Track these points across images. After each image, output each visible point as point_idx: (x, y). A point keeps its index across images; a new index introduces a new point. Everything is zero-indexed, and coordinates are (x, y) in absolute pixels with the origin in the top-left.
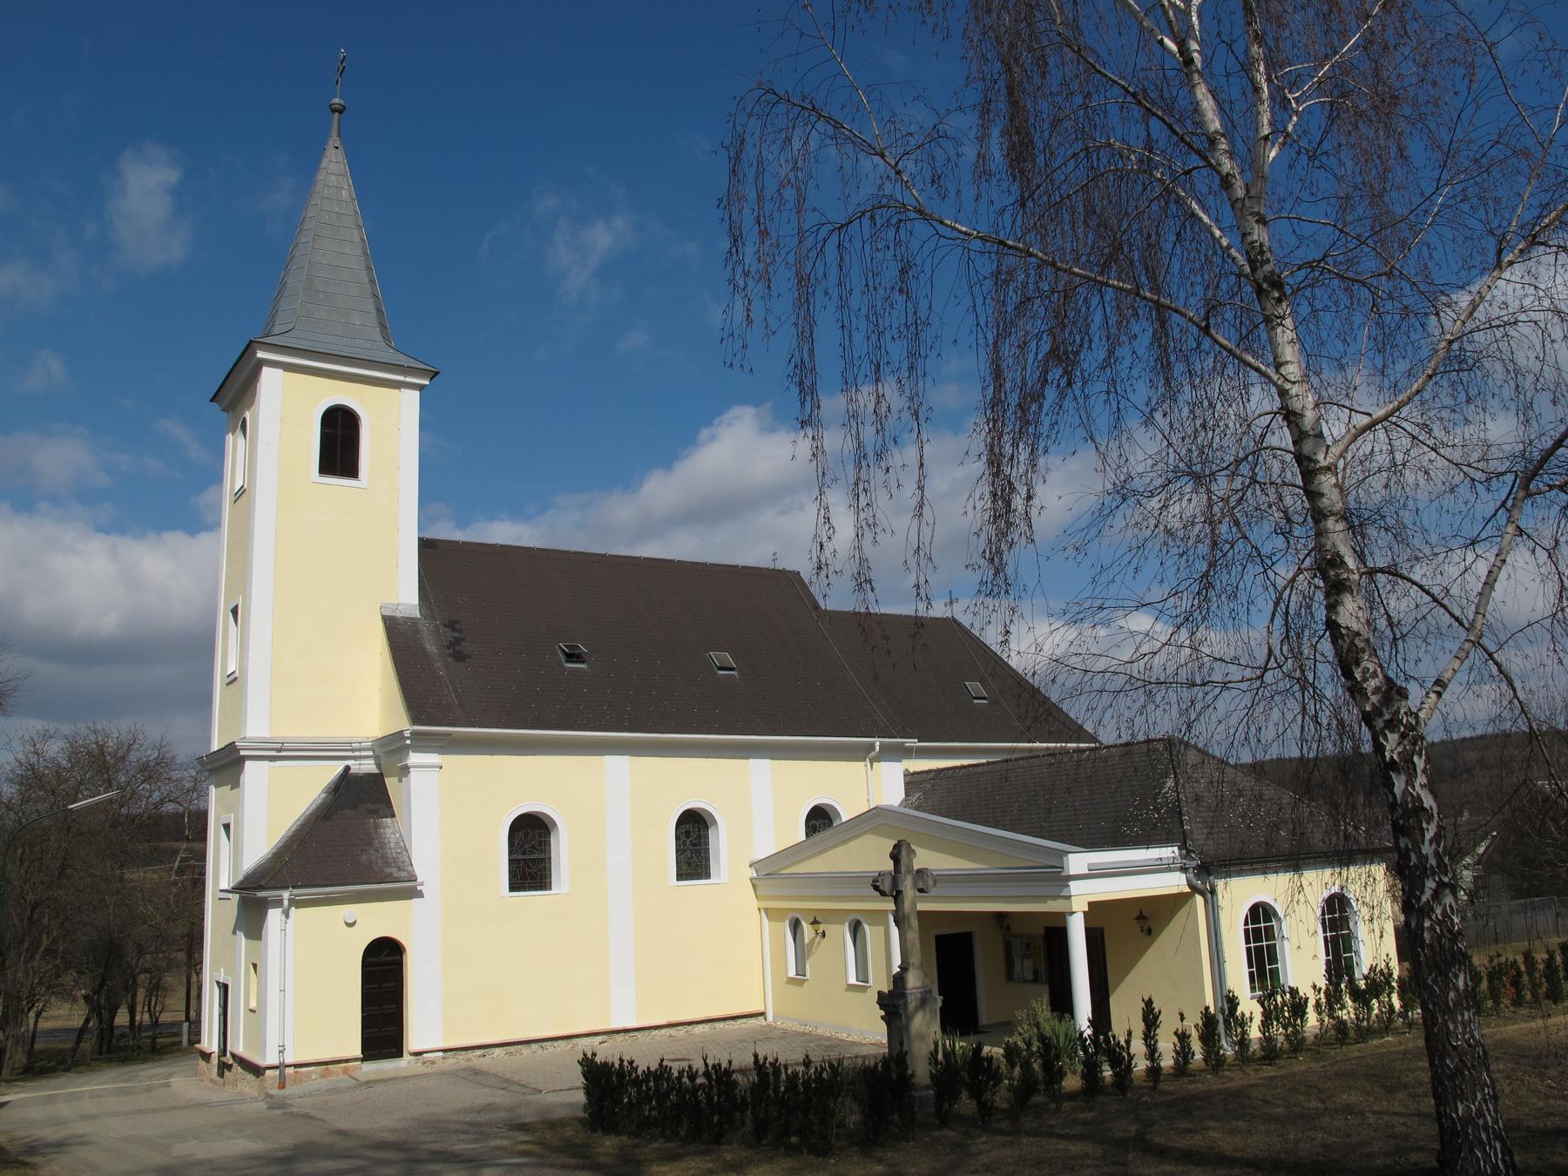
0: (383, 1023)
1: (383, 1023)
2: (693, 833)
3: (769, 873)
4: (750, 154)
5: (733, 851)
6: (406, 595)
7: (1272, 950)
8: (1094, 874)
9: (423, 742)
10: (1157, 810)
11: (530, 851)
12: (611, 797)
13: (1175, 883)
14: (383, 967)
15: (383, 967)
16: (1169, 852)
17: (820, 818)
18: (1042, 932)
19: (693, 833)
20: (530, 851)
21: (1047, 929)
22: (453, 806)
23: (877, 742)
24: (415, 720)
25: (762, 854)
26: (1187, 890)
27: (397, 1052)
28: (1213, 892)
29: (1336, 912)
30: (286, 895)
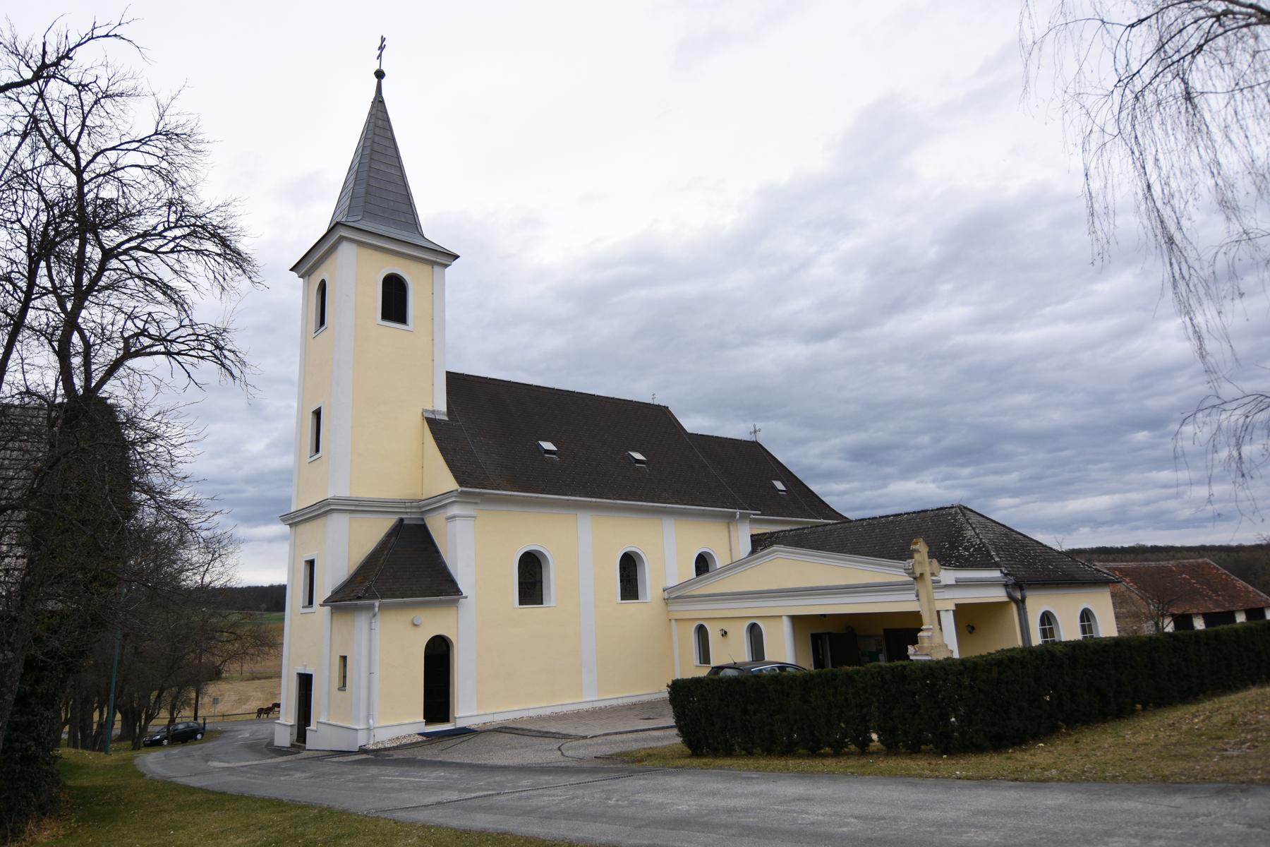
0: (437, 699)
1: (437, 699)
2: (629, 567)
3: (673, 596)
4: (1175, 58)
5: (653, 581)
6: (440, 404)
7: (1090, 626)
8: (960, 584)
9: (463, 498)
10: (967, 549)
11: (531, 577)
12: (582, 543)
13: (999, 595)
14: (438, 657)
15: (438, 657)
16: (996, 574)
17: (703, 564)
18: (882, 632)
19: (629, 567)
20: (531, 577)
21: (885, 630)
22: (479, 545)
23: (738, 512)
24: (461, 484)
25: (671, 584)
26: (1006, 599)
27: (446, 719)
28: (1023, 601)
29: (1086, 616)
30: (377, 603)
